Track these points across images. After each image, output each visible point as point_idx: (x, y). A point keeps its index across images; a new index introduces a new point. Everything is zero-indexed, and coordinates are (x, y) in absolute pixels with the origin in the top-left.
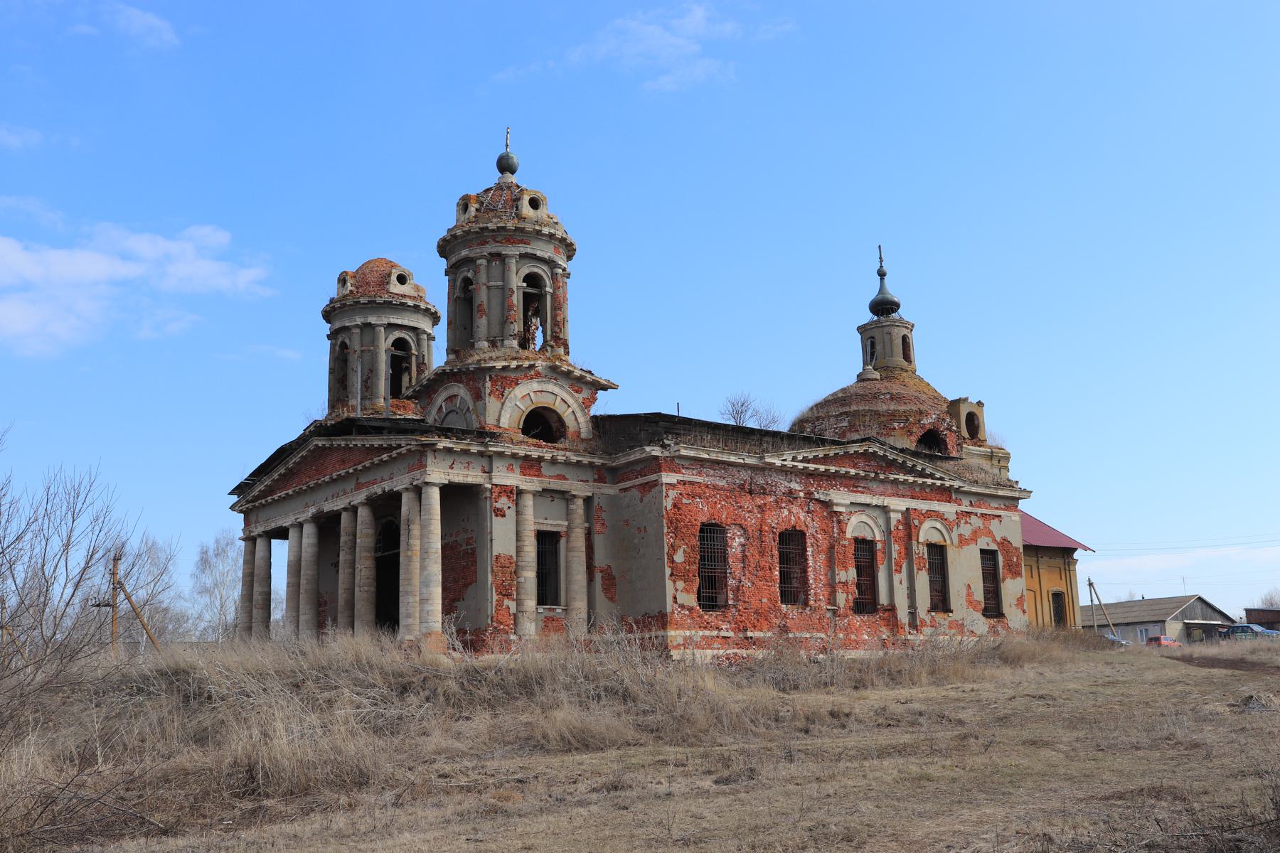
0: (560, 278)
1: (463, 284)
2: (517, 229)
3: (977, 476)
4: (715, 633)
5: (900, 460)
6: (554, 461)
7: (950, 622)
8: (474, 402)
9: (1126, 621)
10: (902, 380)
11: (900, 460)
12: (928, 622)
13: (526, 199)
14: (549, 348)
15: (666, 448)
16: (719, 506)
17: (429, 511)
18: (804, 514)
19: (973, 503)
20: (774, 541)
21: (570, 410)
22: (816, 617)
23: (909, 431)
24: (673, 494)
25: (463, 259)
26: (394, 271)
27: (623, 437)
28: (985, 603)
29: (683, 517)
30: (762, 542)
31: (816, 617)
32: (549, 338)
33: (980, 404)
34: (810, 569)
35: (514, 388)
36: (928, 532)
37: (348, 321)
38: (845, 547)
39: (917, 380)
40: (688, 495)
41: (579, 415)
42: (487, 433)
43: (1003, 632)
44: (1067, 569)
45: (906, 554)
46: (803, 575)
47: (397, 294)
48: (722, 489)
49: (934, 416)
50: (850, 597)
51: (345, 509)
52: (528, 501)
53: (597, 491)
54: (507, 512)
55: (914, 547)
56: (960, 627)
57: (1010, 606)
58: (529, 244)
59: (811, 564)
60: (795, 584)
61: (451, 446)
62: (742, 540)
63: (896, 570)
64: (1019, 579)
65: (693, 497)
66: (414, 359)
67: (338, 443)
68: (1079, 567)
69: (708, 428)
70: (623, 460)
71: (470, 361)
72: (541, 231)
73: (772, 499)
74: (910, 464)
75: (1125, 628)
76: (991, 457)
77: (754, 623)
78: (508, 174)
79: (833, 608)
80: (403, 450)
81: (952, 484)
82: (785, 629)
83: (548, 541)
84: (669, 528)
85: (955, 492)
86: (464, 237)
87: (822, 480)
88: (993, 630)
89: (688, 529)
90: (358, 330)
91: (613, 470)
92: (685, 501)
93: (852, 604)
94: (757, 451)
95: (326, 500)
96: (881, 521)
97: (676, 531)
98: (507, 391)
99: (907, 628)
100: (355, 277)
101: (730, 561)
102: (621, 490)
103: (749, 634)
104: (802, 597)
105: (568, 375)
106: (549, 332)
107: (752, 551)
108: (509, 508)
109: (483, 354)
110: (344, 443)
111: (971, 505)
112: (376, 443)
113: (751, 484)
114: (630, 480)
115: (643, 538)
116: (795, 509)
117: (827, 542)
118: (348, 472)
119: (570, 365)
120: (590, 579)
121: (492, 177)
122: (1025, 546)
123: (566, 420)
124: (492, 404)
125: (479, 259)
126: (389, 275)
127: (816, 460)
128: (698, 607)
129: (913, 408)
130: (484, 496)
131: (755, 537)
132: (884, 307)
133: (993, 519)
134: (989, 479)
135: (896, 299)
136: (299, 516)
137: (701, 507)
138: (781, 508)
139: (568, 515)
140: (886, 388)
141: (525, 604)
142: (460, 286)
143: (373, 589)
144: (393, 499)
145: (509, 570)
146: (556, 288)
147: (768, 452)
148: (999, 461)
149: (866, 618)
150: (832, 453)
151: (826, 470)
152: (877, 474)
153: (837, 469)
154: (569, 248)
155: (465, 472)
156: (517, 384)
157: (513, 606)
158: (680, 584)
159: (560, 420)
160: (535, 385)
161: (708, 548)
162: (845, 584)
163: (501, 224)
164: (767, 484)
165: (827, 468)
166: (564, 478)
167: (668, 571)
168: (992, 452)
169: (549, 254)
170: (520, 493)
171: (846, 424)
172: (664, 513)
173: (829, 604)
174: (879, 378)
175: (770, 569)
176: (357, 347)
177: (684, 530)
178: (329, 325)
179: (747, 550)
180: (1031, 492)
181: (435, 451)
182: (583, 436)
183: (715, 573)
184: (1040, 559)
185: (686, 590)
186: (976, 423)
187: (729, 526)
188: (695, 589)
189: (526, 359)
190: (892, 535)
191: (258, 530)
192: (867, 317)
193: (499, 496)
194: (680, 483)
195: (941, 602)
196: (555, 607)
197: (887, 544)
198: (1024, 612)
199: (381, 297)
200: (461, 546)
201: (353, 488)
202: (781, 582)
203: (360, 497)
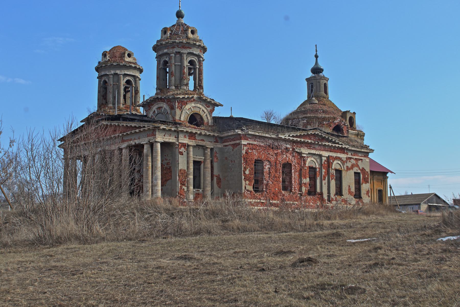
1: (163, 63)
4: (259, 201)
5: (327, 137)
6: (200, 134)
7: (342, 200)
11: (327, 137)
12: (334, 199)
13: (190, 30)
14: (197, 90)
15: (243, 131)
17: (157, 152)
18: (291, 157)
20: (281, 167)
22: (295, 196)
23: (330, 125)
24: (245, 148)
26: (126, 52)
31: (295, 196)
32: (197, 86)
33: (354, 113)
35: (186, 106)
36: (336, 165)
39: (329, 102)
40: (251, 149)
41: (208, 116)
42: (177, 123)
43: (361, 204)
44: (384, 180)
45: (327, 173)
47: (127, 62)
48: (262, 146)
49: (339, 119)
52: (191, 149)
53: (215, 146)
54: (184, 153)
55: (331, 171)
56: (345, 201)
58: (191, 49)
60: (287, 183)
61: (165, 128)
62: (269, 166)
63: (324, 179)
64: (368, 184)
67: (114, 124)
68: (388, 180)
69: (259, 123)
72: (196, 44)
74: (330, 139)
76: (357, 135)
78: (181, 19)
79: (300, 193)
80: (146, 129)
81: (345, 146)
82: (283, 200)
83: (197, 164)
84: (244, 161)
88: (357, 203)
89: (251, 162)
90: (112, 76)
91: (221, 138)
92: (249, 151)
93: (307, 192)
96: (319, 160)
97: (246, 162)
98: (183, 107)
99: (327, 201)
100: (110, 53)
101: (265, 174)
103: (271, 201)
104: (289, 188)
105: (205, 101)
107: (273, 171)
108: (184, 151)
111: (352, 155)
112: (133, 125)
114: (228, 142)
116: (288, 155)
119: (206, 97)
120: (212, 179)
121: (174, 20)
122: (371, 171)
123: (204, 118)
124: (178, 111)
125: (172, 54)
126: (124, 53)
127: (297, 136)
129: (331, 116)
130: (175, 147)
131: (274, 165)
132: (317, 70)
134: (359, 145)
135: (322, 68)
138: (283, 154)
139: (205, 155)
140: (321, 107)
141: (190, 188)
142: (162, 63)
148: (361, 136)
149: (312, 197)
150: (302, 134)
151: (304, 141)
152: (318, 142)
153: (304, 140)
156: (187, 104)
157: (185, 188)
158: (247, 182)
159: (201, 118)
160: (193, 105)
162: (305, 184)
163: (181, 41)
164: (279, 145)
165: (301, 139)
166: (203, 141)
167: (243, 177)
168: (358, 133)
170: (189, 146)
173: (299, 191)
174: (317, 103)
175: (279, 178)
177: (249, 162)
180: (374, 150)
181: (159, 130)
182: (210, 124)
184: (374, 176)
185: (249, 185)
186: (353, 121)
188: (253, 184)
192: (310, 75)
193: (181, 147)
195: (339, 192)
196: (199, 189)
197: (321, 169)
198: (369, 196)
199: (122, 63)
200: (164, 165)
203: (124, 145)
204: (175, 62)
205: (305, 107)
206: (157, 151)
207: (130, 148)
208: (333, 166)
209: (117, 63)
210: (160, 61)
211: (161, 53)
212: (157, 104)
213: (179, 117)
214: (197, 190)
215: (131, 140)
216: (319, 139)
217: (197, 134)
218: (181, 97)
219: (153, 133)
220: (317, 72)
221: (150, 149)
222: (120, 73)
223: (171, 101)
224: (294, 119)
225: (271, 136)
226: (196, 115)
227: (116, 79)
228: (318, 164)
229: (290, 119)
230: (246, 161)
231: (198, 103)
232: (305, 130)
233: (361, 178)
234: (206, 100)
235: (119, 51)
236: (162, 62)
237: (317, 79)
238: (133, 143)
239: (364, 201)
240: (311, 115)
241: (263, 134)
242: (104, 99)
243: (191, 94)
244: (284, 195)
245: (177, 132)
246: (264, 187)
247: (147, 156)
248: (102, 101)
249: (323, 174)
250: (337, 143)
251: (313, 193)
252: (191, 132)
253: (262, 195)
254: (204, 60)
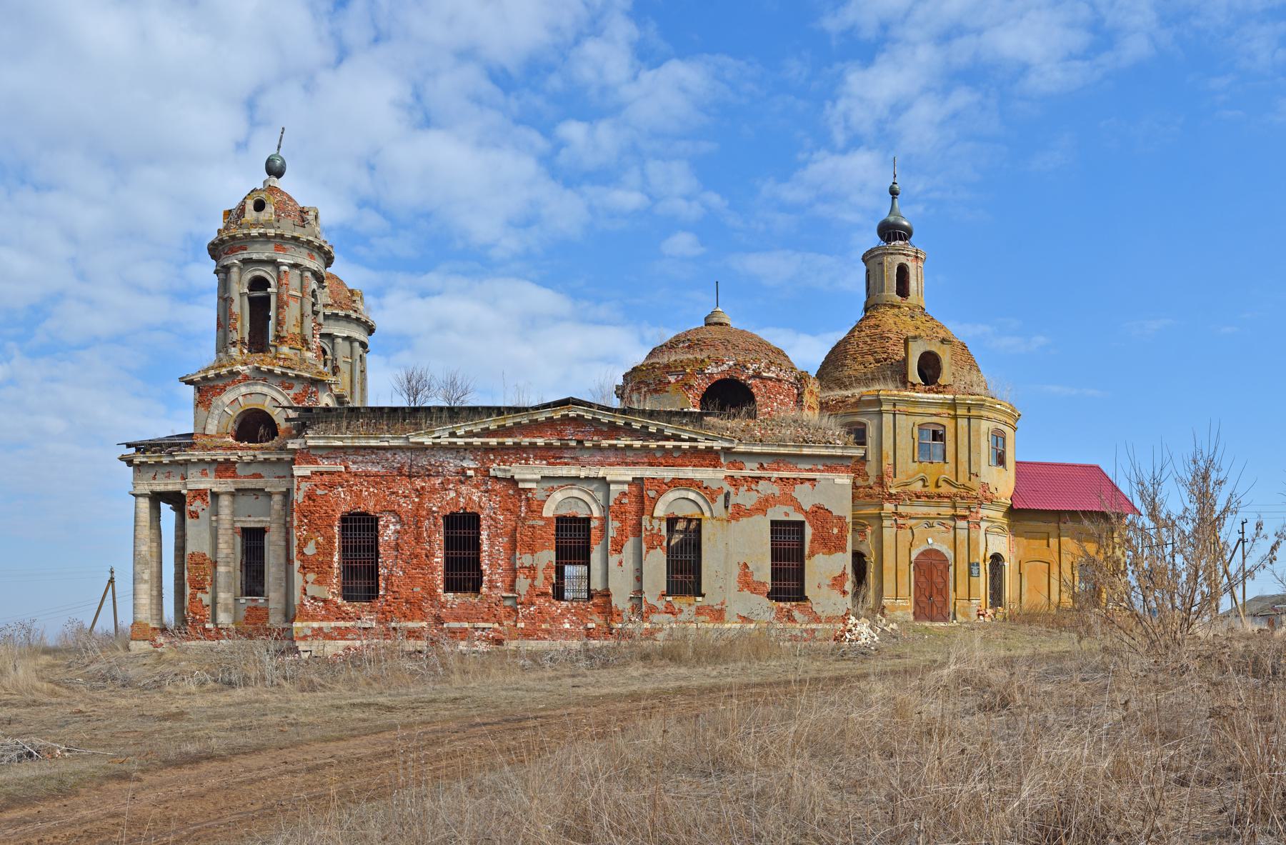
11: (621, 423)
24: (305, 486)
28: (772, 584)
52: (225, 502)
54: (201, 514)
61: (145, 460)
62: (398, 527)
82: (439, 620)
85: (725, 453)
92: (319, 492)
96: (600, 495)
101: (381, 550)
111: (762, 467)
137: (342, 496)
145: (202, 566)
160: (244, 390)
164: (431, 465)
167: (297, 564)
169: (267, 254)
170: (215, 495)
197: (604, 521)
198: (844, 593)
214: (253, 600)
228: (598, 505)
231: (256, 384)
249: (611, 534)
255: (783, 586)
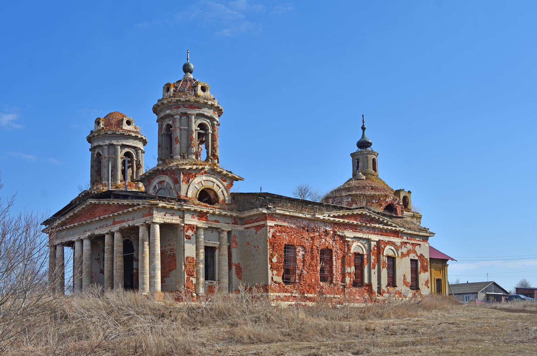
0: (215, 126)
2: (195, 101)
3: (410, 226)
4: (289, 294)
5: (377, 218)
8: (174, 185)
9: (473, 292)
10: (372, 180)
11: (377, 218)
12: (386, 291)
16: (293, 237)
17: (154, 236)
19: (408, 238)
20: (318, 253)
21: (221, 190)
23: (380, 204)
24: (272, 230)
25: (166, 115)
26: (124, 118)
27: (247, 203)
28: (411, 283)
29: (277, 241)
30: (313, 254)
31: (336, 288)
32: (210, 155)
33: (409, 192)
34: (334, 267)
35: (194, 179)
36: (388, 251)
37: (102, 142)
38: (350, 257)
40: (279, 231)
41: (225, 192)
46: (330, 269)
47: (126, 130)
49: (392, 198)
50: (352, 279)
51: (107, 234)
52: (202, 232)
53: (233, 228)
54: (191, 237)
55: (381, 257)
57: (422, 285)
59: (334, 264)
60: (326, 273)
61: (165, 205)
62: (303, 253)
63: (373, 268)
65: (281, 232)
66: (135, 162)
69: (289, 200)
70: (247, 214)
71: (172, 165)
72: (207, 103)
73: (317, 234)
74: (381, 220)
75: (459, 295)
76: (413, 217)
77: (308, 290)
79: (344, 284)
80: (141, 207)
81: (400, 229)
83: (210, 251)
84: (270, 246)
85: (401, 233)
86: (168, 104)
87: (341, 226)
90: (106, 147)
91: (241, 219)
92: (278, 234)
94: (312, 212)
95: (96, 229)
96: (366, 245)
98: (191, 180)
99: (376, 294)
101: (298, 262)
102: (245, 228)
103: (306, 295)
104: (329, 279)
106: (210, 152)
107: (308, 258)
109: (177, 162)
110: (107, 202)
111: (407, 239)
113: (308, 227)
115: (257, 251)
116: (328, 239)
117: (342, 254)
118: (109, 216)
124: (184, 186)
125: (176, 115)
126: (122, 120)
127: (339, 217)
128: (283, 283)
130: (180, 229)
132: (363, 144)
133: (417, 245)
134: (416, 227)
136: (81, 236)
137: (285, 237)
138: (321, 238)
139: (220, 239)
140: (369, 183)
143: (123, 271)
144: (135, 230)
145: (192, 264)
146: (214, 131)
147: (317, 212)
150: (346, 214)
151: (343, 222)
152: (366, 223)
153: (349, 221)
154: (220, 112)
155: (172, 217)
156: (195, 177)
158: (275, 272)
159: (216, 194)
160: (204, 178)
161: (287, 256)
162: (350, 273)
164: (315, 227)
165: (344, 220)
166: (218, 222)
167: (269, 266)
168: (414, 215)
170: (198, 228)
171: (350, 200)
172: (268, 240)
173: (342, 282)
176: (106, 155)
178: (90, 144)
179: (305, 257)
180: (434, 234)
181: (157, 208)
183: (289, 267)
184: (432, 264)
185: (277, 275)
186: (407, 201)
187: (297, 246)
188: (282, 275)
189: (200, 165)
190: (372, 252)
191: (58, 242)
192: (355, 149)
193: (188, 229)
194: (275, 226)
195: (392, 282)
198: (428, 287)
199: (119, 131)
200: (168, 252)
201: (112, 223)
202: (320, 272)
204: (180, 125)
205: (349, 184)
206: (155, 235)
207: (121, 231)
208: (385, 252)
209: (113, 131)
210: (162, 125)
211: (162, 115)
212: (158, 177)
213: (186, 192)
215: (124, 221)
216: (368, 221)
217: (209, 214)
218: (187, 167)
219: (149, 212)
220: (364, 146)
221: (147, 232)
222: (116, 144)
223: (174, 174)
224: (336, 197)
225: (305, 215)
226: (208, 191)
227: (111, 151)
228: (366, 250)
229: (330, 198)
230: (273, 246)
231: (210, 176)
232: (350, 209)
233: (419, 266)
234: (221, 172)
235: (115, 118)
236: (164, 126)
237: (364, 154)
238: (125, 225)
239: (422, 293)
240: (357, 193)
241: (295, 213)
242: (99, 176)
243: (201, 165)
244: (322, 287)
245: (182, 213)
246: (297, 278)
247: (143, 241)
248: (96, 177)
250: (389, 225)
251: (360, 284)
252: (201, 211)
253: (294, 287)
254: (220, 124)
255: (288, 275)
